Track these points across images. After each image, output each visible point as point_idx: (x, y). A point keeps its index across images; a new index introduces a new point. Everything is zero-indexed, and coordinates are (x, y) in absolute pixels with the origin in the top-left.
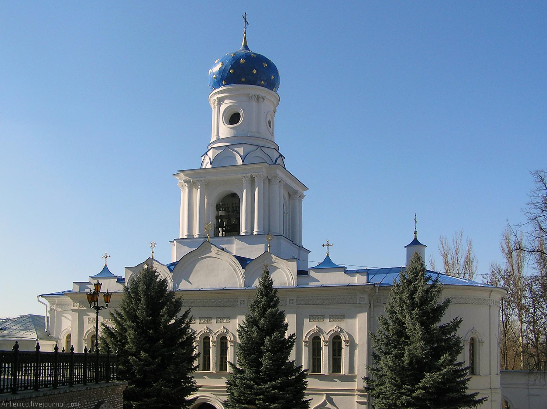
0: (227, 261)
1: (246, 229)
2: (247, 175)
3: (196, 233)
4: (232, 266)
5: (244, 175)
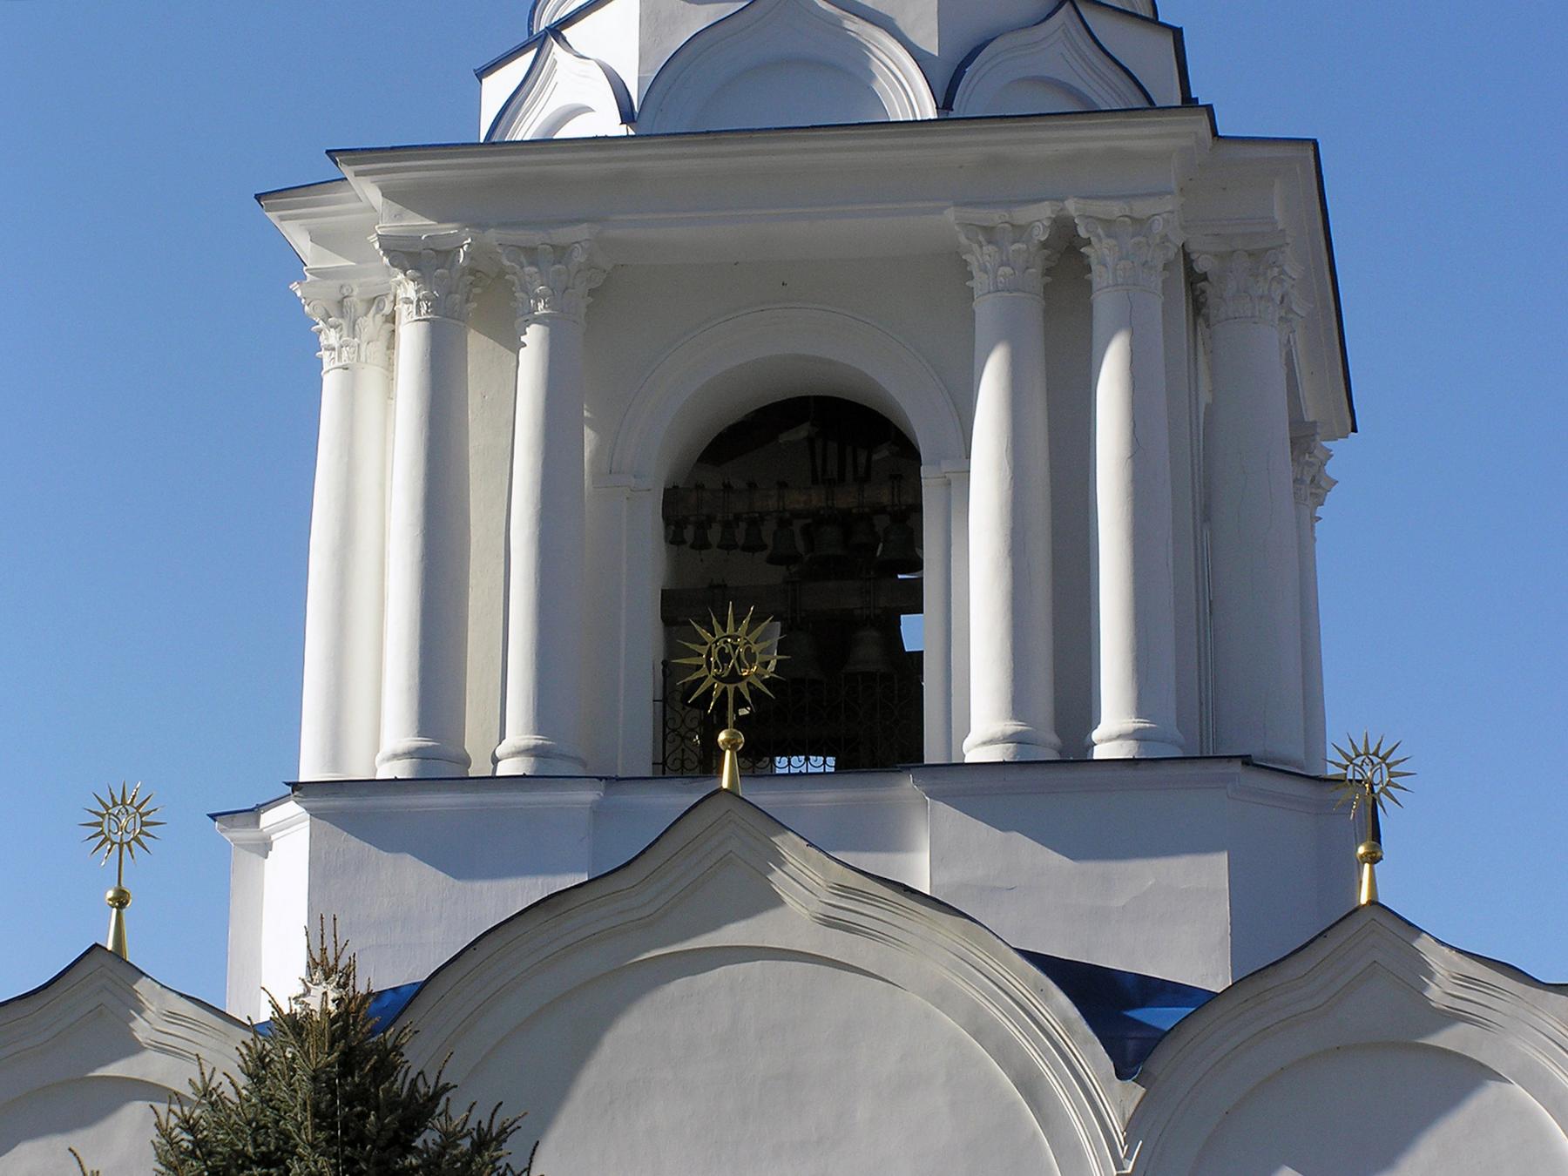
0: (943, 997)
1: (1140, 712)
2: (1024, 215)
3: (505, 736)
4: (1004, 1052)
5: (995, 217)
